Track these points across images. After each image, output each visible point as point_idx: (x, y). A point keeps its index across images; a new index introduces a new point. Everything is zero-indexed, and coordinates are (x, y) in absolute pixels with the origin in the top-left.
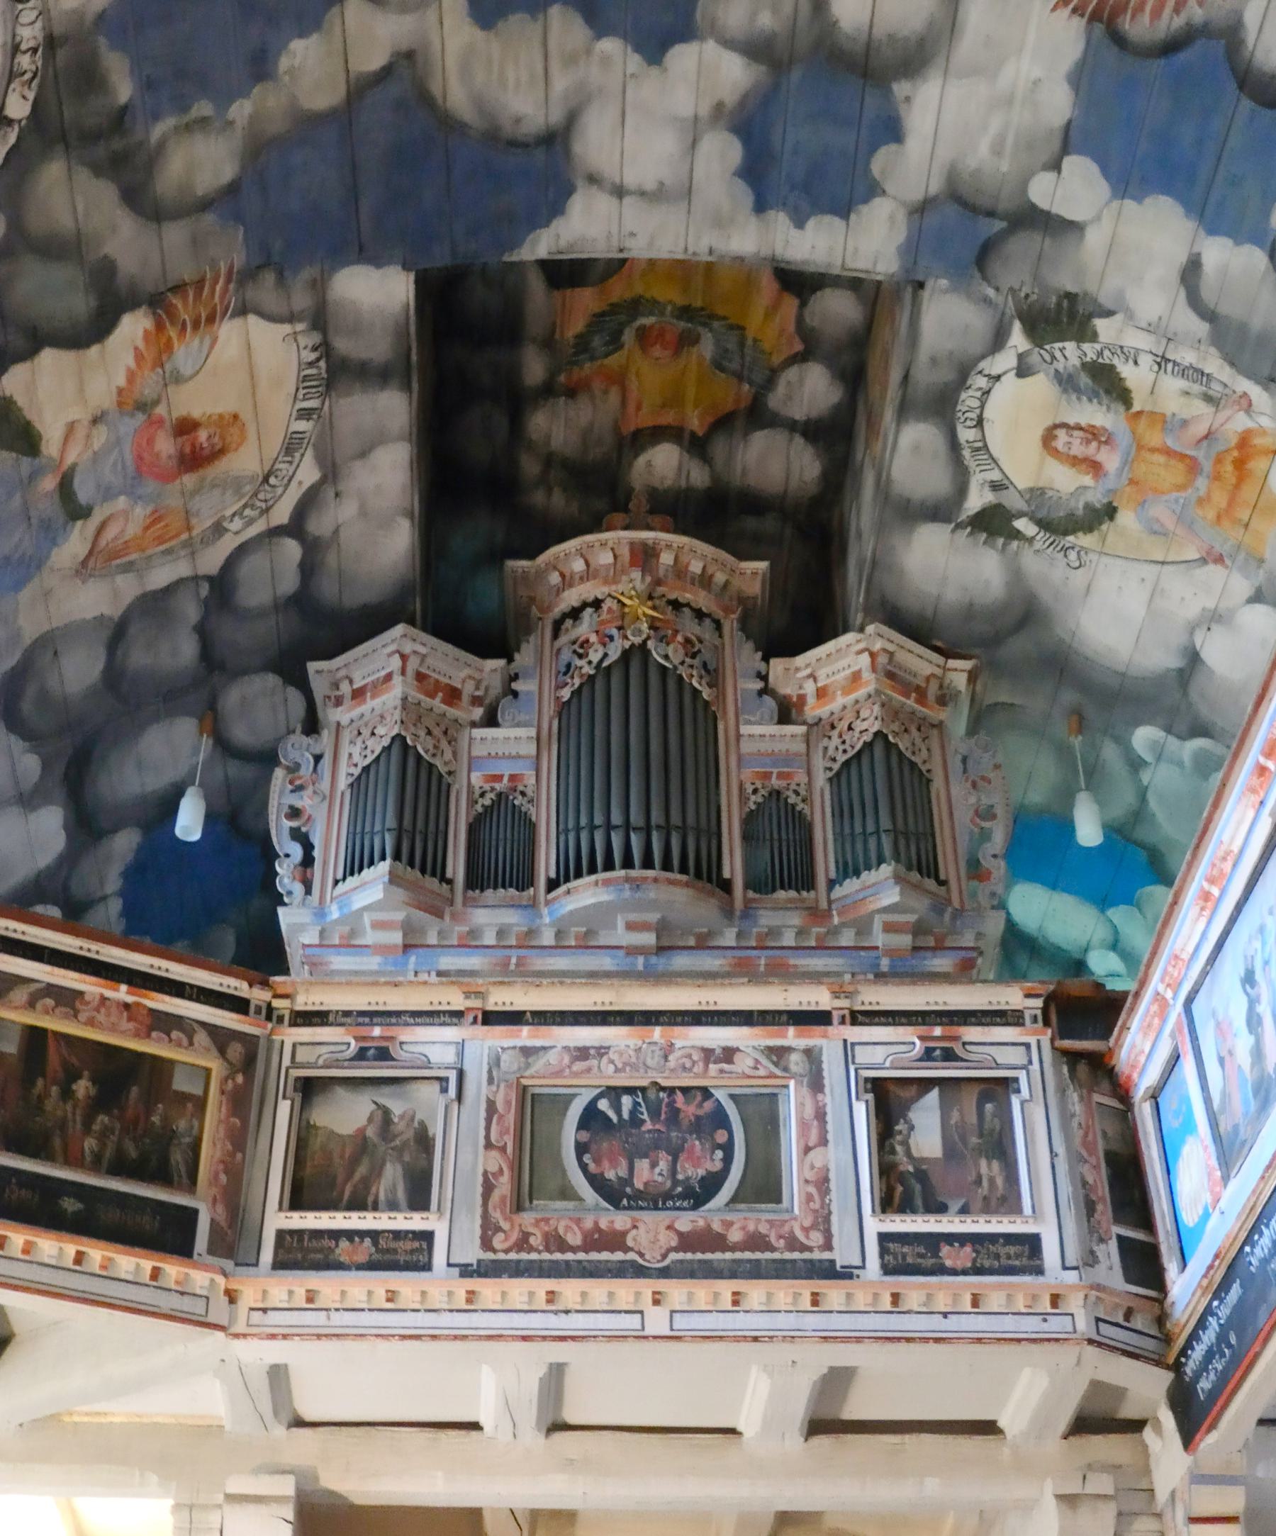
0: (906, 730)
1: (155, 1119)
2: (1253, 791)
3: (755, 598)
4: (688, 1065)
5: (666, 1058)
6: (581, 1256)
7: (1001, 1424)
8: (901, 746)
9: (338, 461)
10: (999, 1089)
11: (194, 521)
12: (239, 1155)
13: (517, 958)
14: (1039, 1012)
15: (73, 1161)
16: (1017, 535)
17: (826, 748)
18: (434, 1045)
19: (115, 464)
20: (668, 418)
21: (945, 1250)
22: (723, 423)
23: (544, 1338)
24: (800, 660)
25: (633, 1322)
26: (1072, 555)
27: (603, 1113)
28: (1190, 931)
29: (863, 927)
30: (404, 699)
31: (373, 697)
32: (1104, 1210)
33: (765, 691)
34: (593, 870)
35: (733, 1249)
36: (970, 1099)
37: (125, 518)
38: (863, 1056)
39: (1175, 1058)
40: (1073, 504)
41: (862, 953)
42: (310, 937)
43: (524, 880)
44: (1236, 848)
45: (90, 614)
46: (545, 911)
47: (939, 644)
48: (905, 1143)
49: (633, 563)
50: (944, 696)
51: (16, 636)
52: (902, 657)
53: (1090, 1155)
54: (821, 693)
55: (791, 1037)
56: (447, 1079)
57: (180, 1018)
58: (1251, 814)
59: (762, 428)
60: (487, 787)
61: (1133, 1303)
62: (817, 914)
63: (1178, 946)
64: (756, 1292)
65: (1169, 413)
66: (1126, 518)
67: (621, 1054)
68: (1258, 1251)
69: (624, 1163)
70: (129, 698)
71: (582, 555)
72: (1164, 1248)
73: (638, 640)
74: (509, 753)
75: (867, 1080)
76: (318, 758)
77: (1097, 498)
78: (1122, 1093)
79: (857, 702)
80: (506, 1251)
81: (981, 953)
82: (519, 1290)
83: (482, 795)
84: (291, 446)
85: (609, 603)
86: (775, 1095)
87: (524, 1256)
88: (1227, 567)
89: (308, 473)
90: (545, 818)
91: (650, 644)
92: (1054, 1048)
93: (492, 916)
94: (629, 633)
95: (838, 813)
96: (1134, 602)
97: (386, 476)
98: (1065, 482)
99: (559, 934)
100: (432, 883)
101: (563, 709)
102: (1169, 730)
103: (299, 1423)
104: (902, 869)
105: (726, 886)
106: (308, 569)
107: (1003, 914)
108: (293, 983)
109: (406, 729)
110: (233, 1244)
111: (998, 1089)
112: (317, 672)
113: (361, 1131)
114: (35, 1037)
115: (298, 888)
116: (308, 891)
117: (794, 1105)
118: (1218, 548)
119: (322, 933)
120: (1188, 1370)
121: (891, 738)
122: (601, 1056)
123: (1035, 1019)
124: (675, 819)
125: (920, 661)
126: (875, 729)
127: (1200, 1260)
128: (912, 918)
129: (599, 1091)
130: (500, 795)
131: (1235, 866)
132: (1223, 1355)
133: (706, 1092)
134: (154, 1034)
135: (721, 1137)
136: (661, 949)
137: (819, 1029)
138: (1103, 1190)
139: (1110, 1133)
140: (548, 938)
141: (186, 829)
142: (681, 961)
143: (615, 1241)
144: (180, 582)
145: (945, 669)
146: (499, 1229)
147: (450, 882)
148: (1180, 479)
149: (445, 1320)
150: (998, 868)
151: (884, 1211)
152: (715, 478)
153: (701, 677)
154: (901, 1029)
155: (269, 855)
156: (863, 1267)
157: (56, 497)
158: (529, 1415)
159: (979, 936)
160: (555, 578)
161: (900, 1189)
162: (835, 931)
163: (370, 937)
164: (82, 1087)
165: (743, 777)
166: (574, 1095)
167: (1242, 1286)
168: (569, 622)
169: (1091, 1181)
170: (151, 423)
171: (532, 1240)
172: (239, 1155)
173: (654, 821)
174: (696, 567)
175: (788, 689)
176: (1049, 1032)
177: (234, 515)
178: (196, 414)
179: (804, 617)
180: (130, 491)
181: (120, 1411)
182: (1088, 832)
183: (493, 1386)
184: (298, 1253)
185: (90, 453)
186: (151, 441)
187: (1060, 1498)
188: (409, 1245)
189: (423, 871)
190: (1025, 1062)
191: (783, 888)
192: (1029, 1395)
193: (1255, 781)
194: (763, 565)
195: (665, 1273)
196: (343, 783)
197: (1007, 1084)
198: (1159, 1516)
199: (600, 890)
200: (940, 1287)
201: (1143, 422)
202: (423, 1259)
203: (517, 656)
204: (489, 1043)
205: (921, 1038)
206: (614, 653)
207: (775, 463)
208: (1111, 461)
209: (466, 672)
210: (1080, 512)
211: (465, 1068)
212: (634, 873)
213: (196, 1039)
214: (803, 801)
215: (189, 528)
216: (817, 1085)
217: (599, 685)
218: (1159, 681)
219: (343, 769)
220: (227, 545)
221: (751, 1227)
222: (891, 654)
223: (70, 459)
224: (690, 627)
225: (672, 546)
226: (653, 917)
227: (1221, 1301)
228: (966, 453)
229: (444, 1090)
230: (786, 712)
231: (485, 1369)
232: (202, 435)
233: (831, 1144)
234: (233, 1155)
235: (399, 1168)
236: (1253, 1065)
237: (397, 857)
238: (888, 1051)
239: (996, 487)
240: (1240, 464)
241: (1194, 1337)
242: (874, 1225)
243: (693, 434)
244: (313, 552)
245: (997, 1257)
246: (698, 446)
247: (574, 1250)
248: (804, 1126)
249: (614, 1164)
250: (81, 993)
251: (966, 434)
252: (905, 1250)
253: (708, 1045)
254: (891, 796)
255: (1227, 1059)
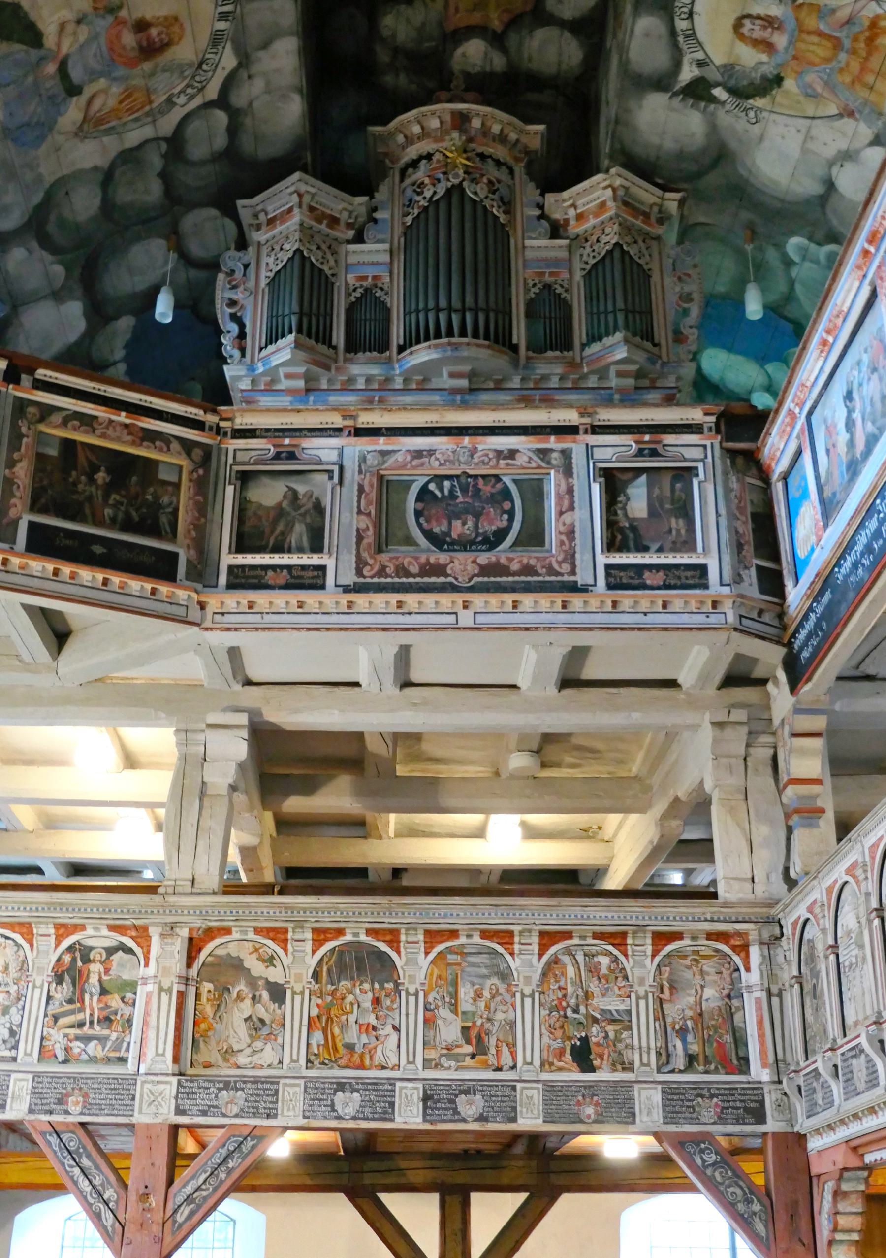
0: (635, 242)
1: (149, 497)
2: (859, 267)
3: (536, 152)
4: (486, 460)
5: (472, 456)
6: (418, 580)
7: (679, 681)
8: (632, 253)
9: (249, 50)
10: (685, 474)
11: (153, 97)
12: (203, 520)
13: (379, 393)
14: (713, 425)
15: (98, 522)
16: (713, 100)
17: (581, 255)
18: (324, 449)
19: (95, 55)
20: (476, 18)
21: (647, 574)
22: (515, 22)
23: (396, 629)
24: (566, 194)
25: (451, 619)
26: (752, 114)
27: (432, 492)
28: (813, 366)
29: (603, 373)
30: (302, 224)
31: (281, 224)
32: (749, 550)
33: (543, 216)
34: (427, 339)
35: (514, 574)
36: (666, 480)
37: (105, 94)
38: (598, 454)
39: (799, 453)
40: (753, 75)
41: (603, 392)
42: (245, 385)
43: (383, 346)
44: (845, 309)
45: (88, 164)
46: (397, 366)
47: (659, 181)
48: (624, 509)
49: (455, 127)
50: (661, 218)
51: (39, 179)
52: (634, 190)
53: (741, 513)
54: (580, 217)
55: (552, 442)
56: (332, 471)
57: (161, 433)
58: (857, 284)
59: (543, 26)
60: (358, 284)
61: (763, 606)
62: (573, 365)
63: (805, 377)
64: (527, 600)
65: (822, 4)
66: (789, 84)
67: (443, 454)
68: (843, 571)
69: (445, 523)
70: (120, 224)
71: (419, 122)
72: (785, 572)
73: (456, 181)
74: (371, 261)
75: (601, 469)
76: (246, 266)
77: (769, 70)
78: (764, 475)
79: (603, 222)
80: (372, 577)
81: (680, 391)
82: (379, 600)
83: (355, 290)
84: (216, 40)
85: (437, 156)
86: (542, 480)
87: (383, 580)
88: (856, 120)
89: (229, 61)
90: (396, 304)
91: (465, 184)
92: (721, 447)
93: (363, 369)
94: (450, 177)
95: (589, 299)
96: (792, 145)
97: (284, 59)
98: (749, 57)
99: (406, 381)
100: (322, 348)
101: (407, 231)
102: (810, 239)
103: (249, 683)
104: (629, 335)
105: (515, 348)
106: (233, 130)
107: (693, 365)
108: (233, 411)
109: (304, 245)
110: (202, 574)
111: (685, 474)
112: (244, 207)
113: (280, 504)
114: (68, 446)
115: (237, 353)
116: (243, 355)
117: (553, 484)
118: (852, 106)
119: (253, 382)
120: (796, 647)
121: (625, 248)
122: (431, 455)
123: (710, 429)
124: (482, 303)
125: (646, 194)
126: (613, 242)
127: (806, 579)
128: (634, 368)
129: (427, 478)
130: (366, 290)
131: (844, 320)
132: (817, 636)
133: (497, 478)
134: (145, 444)
135: (507, 505)
136: (471, 390)
137: (570, 437)
138: (749, 537)
139: (755, 501)
140: (398, 383)
141: (163, 315)
142: (484, 397)
143: (439, 570)
144: (147, 142)
145: (662, 198)
146: (366, 564)
147: (335, 348)
148: (826, 53)
149: (334, 618)
150: (693, 335)
151: (609, 551)
152: (510, 64)
153: (499, 207)
154: (623, 437)
155: (219, 332)
156: (595, 585)
157: (58, 78)
158: (389, 676)
159: (679, 379)
160: (400, 139)
161: (619, 537)
162: (584, 377)
163: (284, 384)
164: (101, 476)
165: (526, 276)
166: (414, 481)
167: (832, 593)
168: (410, 170)
169: (741, 531)
170: (118, 24)
171: (388, 570)
172: (203, 520)
173: (467, 306)
174: (496, 129)
175: (557, 216)
176: (719, 437)
177: (180, 93)
178: (148, 17)
179: (567, 165)
180: (106, 74)
181: (141, 674)
182: (754, 308)
183: (366, 659)
184: (242, 579)
185: (77, 46)
186: (118, 36)
187: (713, 723)
188: (310, 574)
189: (317, 341)
190: (702, 456)
191: (552, 349)
192: (696, 662)
193: (861, 261)
194: (541, 127)
195: (471, 589)
196: (263, 282)
197: (691, 471)
198: (774, 734)
199: (432, 350)
200: (643, 597)
201: (803, 14)
202: (320, 582)
203: (376, 195)
204: (358, 448)
205: (636, 442)
206: (441, 191)
207: (551, 51)
208: (780, 40)
209: (344, 205)
210: (758, 81)
211: (344, 464)
212: (453, 340)
213: (172, 446)
214: (566, 291)
215: (151, 102)
216: (568, 471)
217: (431, 211)
218: (808, 202)
219: (263, 273)
220: (176, 115)
221: (525, 561)
222: (627, 189)
223: (65, 50)
224: (494, 173)
225: (485, 116)
226: (466, 368)
227: (818, 602)
228: (681, 39)
229: (331, 478)
230: (556, 230)
231: (361, 648)
232: (154, 32)
233: (577, 510)
234: (198, 519)
235: (303, 527)
236: (847, 453)
237: (300, 331)
238: (613, 450)
239: (701, 64)
240: (870, 41)
241: (801, 625)
242: (603, 560)
243: (494, 32)
244: (235, 115)
245: (679, 578)
246: (497, 40)
247: (414, 576)
248: (559, 498)
249: (439, 524)
250: (96, 417)
251: (681, 25)
252: (622, 574)
253: (499, 448)
254: (624, 286)
255: (832, 450)
